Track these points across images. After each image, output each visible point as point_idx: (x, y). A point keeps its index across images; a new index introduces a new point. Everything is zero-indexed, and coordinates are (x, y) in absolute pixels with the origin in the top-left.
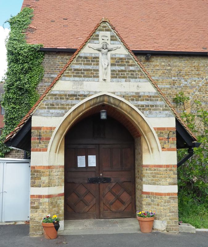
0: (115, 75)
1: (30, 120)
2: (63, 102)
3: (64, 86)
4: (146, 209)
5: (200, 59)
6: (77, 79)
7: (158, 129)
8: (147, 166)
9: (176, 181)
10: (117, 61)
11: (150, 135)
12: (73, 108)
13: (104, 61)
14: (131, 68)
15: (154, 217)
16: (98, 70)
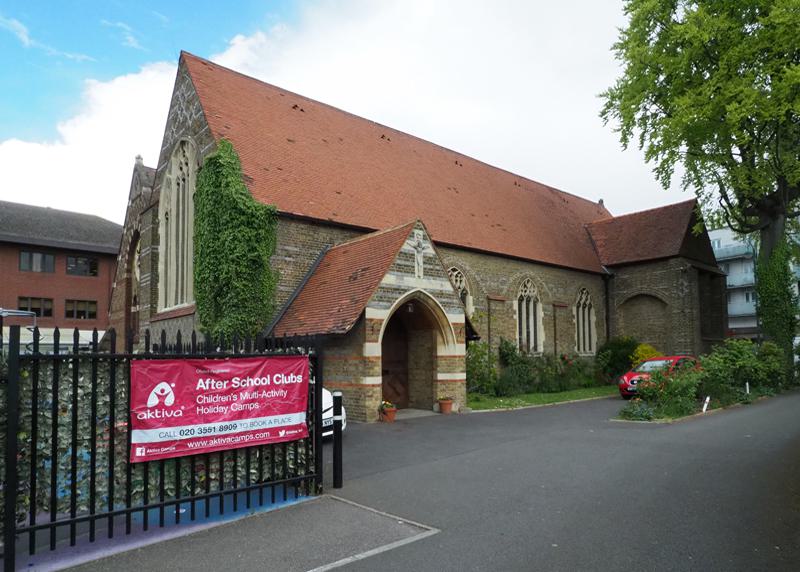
0: (427, 273)
1: (364, 311)
2: (390, 295)
3: (390, 279)
4: (441, 396)
5: (726, 255)
6: (399, 273)
7: (454, 324)
8: (442, 357)
9: (464, 369)
10: (428, 260)
11: (448, 330)
12: (397, 301)
13: (419, 258)
14: (438, 268)
15: (449, 400)
16: (424, 263)
